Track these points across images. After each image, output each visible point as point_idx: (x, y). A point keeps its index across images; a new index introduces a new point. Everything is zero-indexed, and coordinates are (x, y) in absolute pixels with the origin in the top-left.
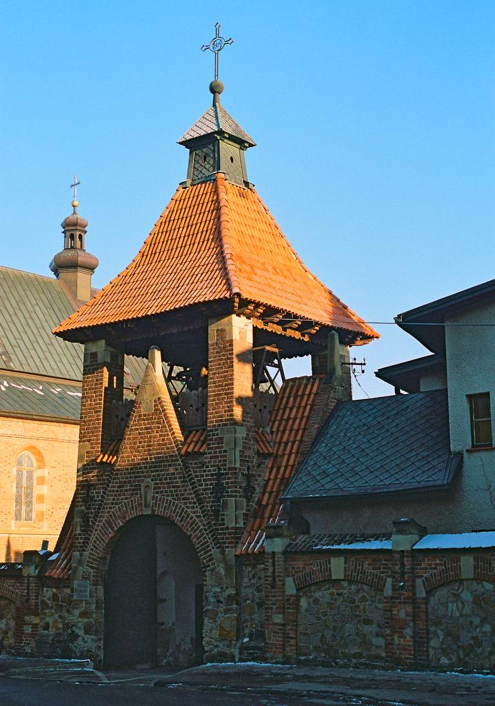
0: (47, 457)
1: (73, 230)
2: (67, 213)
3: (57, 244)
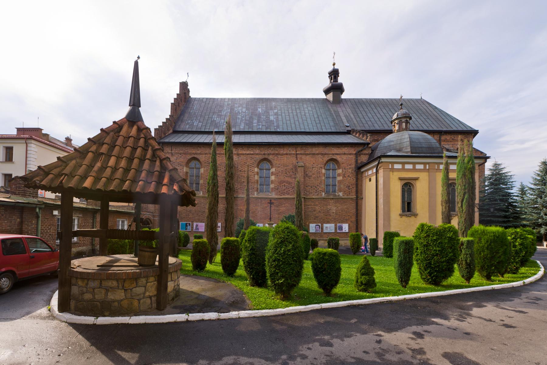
0: (274, 162)
1: (334, 74)
2: (331, 68)
3: (176, 90)
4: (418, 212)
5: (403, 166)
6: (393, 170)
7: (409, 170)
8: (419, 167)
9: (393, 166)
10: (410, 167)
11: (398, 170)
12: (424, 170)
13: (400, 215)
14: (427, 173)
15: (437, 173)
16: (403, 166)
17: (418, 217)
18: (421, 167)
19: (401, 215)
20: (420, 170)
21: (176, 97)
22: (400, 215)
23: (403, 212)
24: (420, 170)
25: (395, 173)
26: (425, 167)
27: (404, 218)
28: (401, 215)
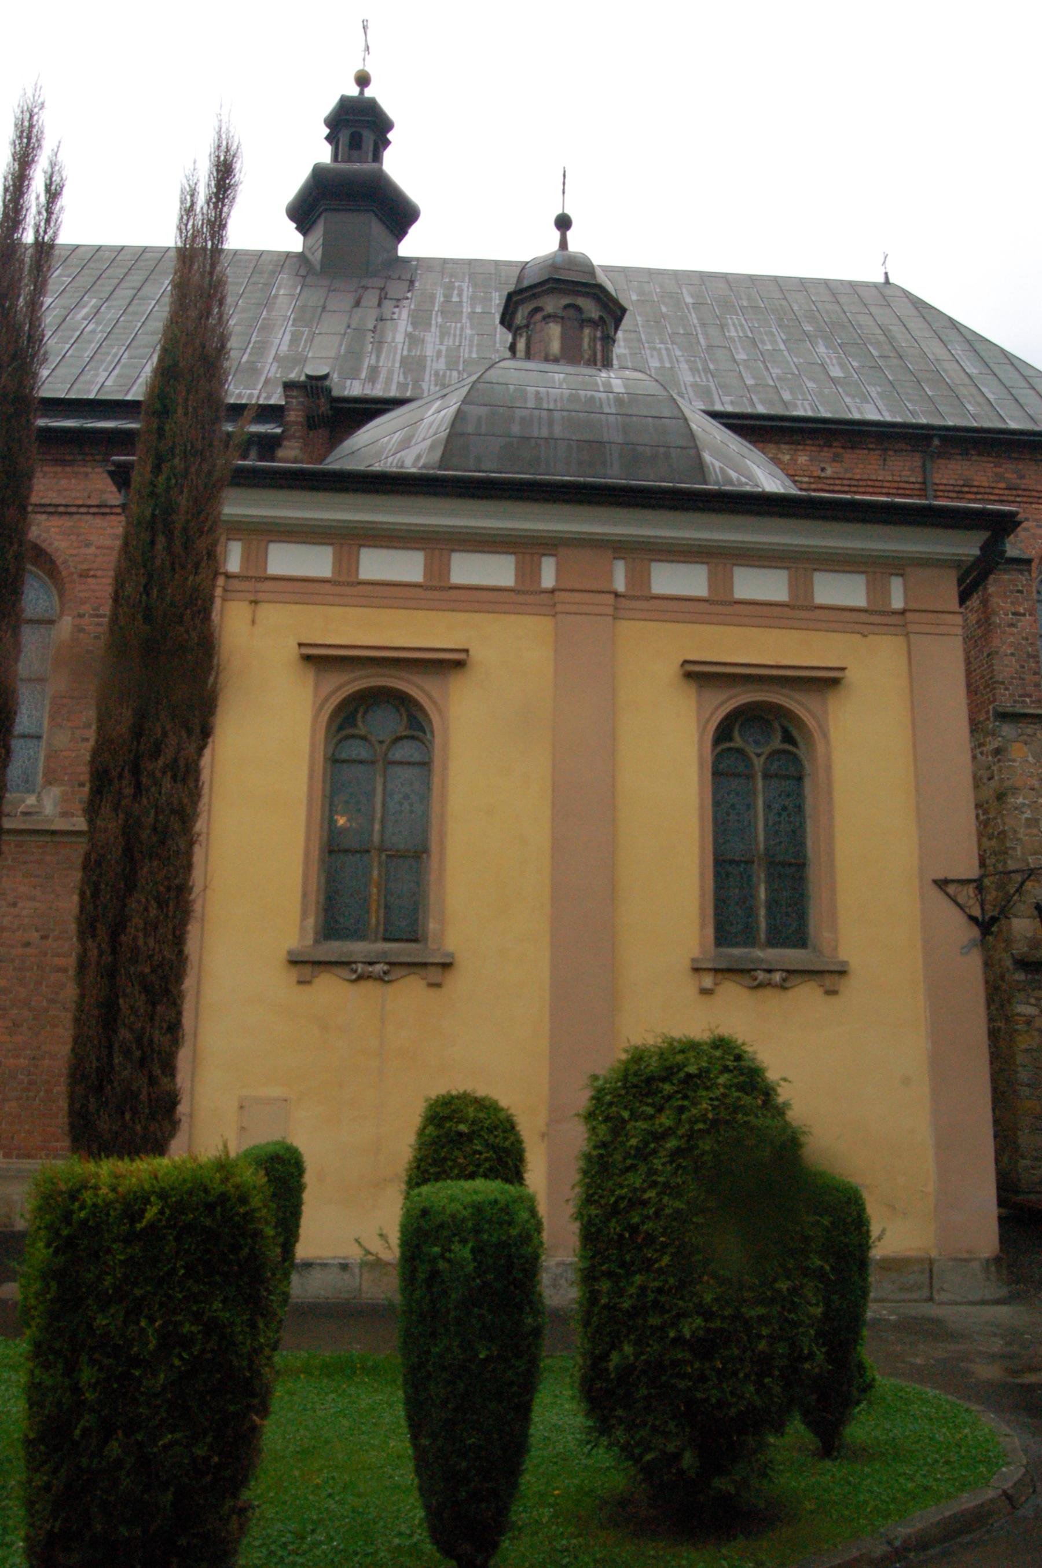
4: (843, 955)
5: (437, 571)
6: (640, 600)
7: (762, 613)
8: (469, 569)
9: (639, 579)
10: (406, 567)
11: (301, 589)
12: (874, 619)
13: (295, 962)
14: (545, 624)
15: (627, 628)
16: (437, 571)
17: (459, 983)
18: (497, 571)
19: (304, 965)
20: (840, 618)
21: (327, 131)
22: (295, 962)
23: (723, 936)
24: (840, 618)
25: (273, 614)
26: (528, 573)
27: (330, 989)
28: (304, 965)
